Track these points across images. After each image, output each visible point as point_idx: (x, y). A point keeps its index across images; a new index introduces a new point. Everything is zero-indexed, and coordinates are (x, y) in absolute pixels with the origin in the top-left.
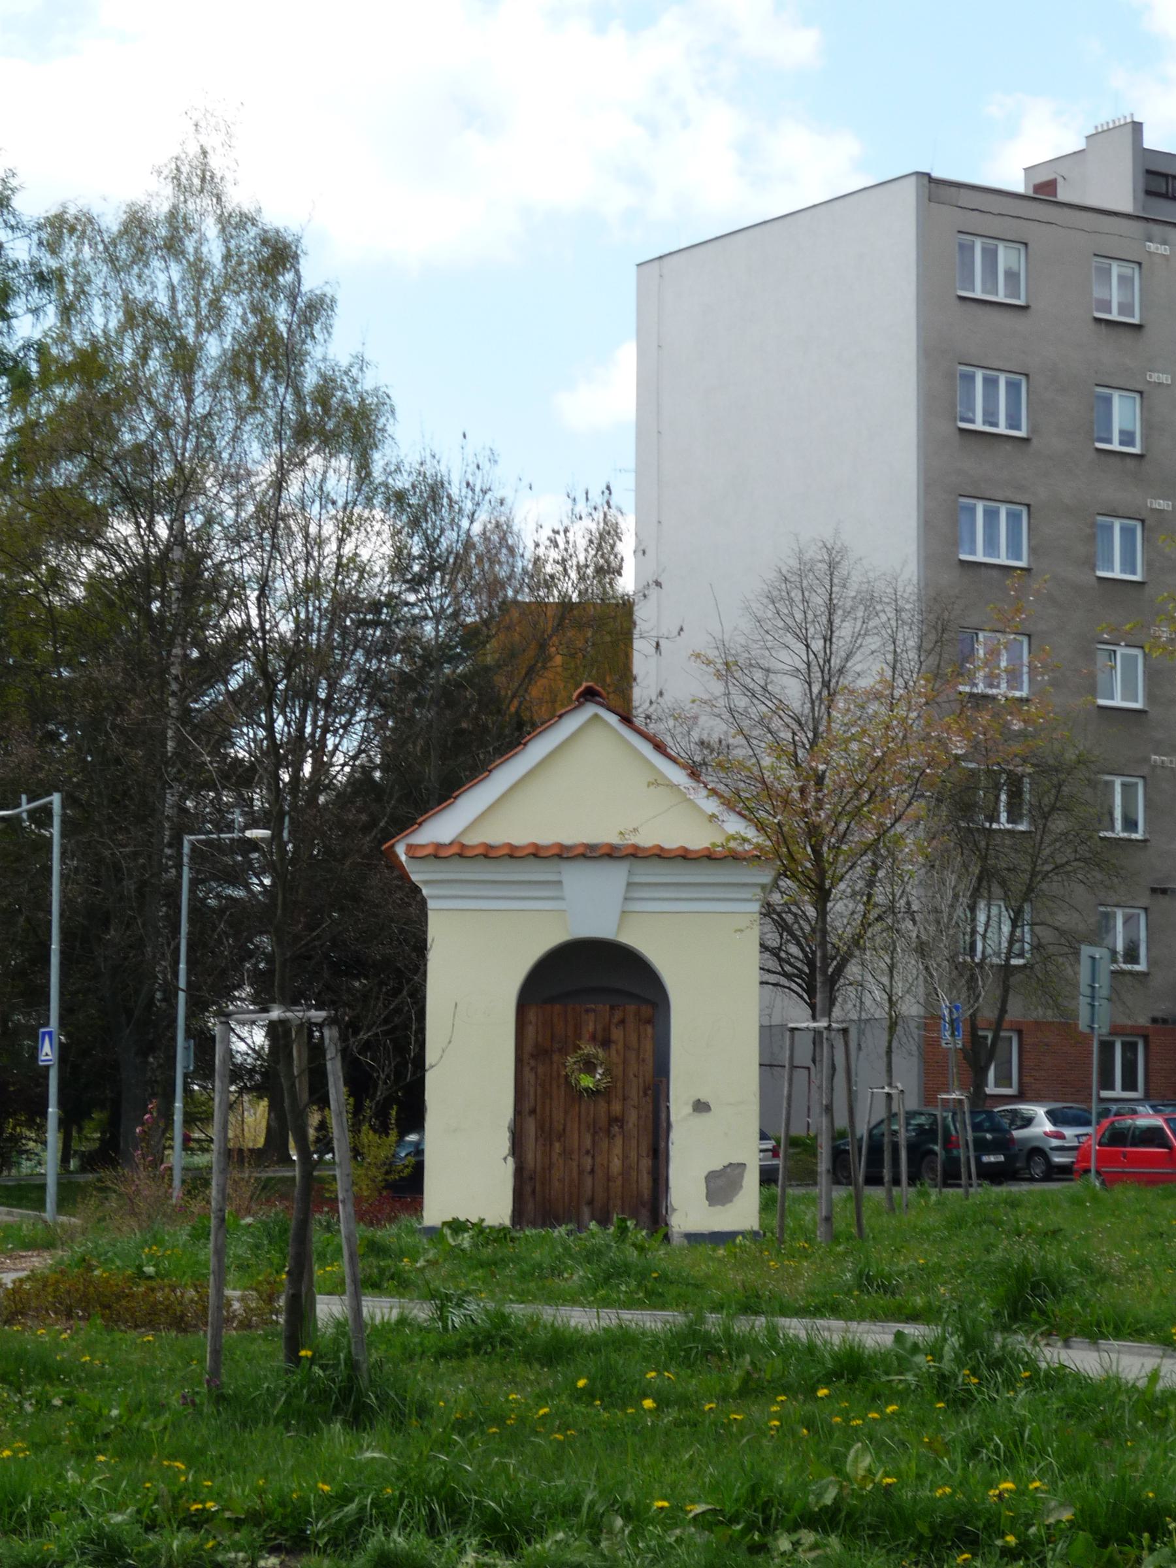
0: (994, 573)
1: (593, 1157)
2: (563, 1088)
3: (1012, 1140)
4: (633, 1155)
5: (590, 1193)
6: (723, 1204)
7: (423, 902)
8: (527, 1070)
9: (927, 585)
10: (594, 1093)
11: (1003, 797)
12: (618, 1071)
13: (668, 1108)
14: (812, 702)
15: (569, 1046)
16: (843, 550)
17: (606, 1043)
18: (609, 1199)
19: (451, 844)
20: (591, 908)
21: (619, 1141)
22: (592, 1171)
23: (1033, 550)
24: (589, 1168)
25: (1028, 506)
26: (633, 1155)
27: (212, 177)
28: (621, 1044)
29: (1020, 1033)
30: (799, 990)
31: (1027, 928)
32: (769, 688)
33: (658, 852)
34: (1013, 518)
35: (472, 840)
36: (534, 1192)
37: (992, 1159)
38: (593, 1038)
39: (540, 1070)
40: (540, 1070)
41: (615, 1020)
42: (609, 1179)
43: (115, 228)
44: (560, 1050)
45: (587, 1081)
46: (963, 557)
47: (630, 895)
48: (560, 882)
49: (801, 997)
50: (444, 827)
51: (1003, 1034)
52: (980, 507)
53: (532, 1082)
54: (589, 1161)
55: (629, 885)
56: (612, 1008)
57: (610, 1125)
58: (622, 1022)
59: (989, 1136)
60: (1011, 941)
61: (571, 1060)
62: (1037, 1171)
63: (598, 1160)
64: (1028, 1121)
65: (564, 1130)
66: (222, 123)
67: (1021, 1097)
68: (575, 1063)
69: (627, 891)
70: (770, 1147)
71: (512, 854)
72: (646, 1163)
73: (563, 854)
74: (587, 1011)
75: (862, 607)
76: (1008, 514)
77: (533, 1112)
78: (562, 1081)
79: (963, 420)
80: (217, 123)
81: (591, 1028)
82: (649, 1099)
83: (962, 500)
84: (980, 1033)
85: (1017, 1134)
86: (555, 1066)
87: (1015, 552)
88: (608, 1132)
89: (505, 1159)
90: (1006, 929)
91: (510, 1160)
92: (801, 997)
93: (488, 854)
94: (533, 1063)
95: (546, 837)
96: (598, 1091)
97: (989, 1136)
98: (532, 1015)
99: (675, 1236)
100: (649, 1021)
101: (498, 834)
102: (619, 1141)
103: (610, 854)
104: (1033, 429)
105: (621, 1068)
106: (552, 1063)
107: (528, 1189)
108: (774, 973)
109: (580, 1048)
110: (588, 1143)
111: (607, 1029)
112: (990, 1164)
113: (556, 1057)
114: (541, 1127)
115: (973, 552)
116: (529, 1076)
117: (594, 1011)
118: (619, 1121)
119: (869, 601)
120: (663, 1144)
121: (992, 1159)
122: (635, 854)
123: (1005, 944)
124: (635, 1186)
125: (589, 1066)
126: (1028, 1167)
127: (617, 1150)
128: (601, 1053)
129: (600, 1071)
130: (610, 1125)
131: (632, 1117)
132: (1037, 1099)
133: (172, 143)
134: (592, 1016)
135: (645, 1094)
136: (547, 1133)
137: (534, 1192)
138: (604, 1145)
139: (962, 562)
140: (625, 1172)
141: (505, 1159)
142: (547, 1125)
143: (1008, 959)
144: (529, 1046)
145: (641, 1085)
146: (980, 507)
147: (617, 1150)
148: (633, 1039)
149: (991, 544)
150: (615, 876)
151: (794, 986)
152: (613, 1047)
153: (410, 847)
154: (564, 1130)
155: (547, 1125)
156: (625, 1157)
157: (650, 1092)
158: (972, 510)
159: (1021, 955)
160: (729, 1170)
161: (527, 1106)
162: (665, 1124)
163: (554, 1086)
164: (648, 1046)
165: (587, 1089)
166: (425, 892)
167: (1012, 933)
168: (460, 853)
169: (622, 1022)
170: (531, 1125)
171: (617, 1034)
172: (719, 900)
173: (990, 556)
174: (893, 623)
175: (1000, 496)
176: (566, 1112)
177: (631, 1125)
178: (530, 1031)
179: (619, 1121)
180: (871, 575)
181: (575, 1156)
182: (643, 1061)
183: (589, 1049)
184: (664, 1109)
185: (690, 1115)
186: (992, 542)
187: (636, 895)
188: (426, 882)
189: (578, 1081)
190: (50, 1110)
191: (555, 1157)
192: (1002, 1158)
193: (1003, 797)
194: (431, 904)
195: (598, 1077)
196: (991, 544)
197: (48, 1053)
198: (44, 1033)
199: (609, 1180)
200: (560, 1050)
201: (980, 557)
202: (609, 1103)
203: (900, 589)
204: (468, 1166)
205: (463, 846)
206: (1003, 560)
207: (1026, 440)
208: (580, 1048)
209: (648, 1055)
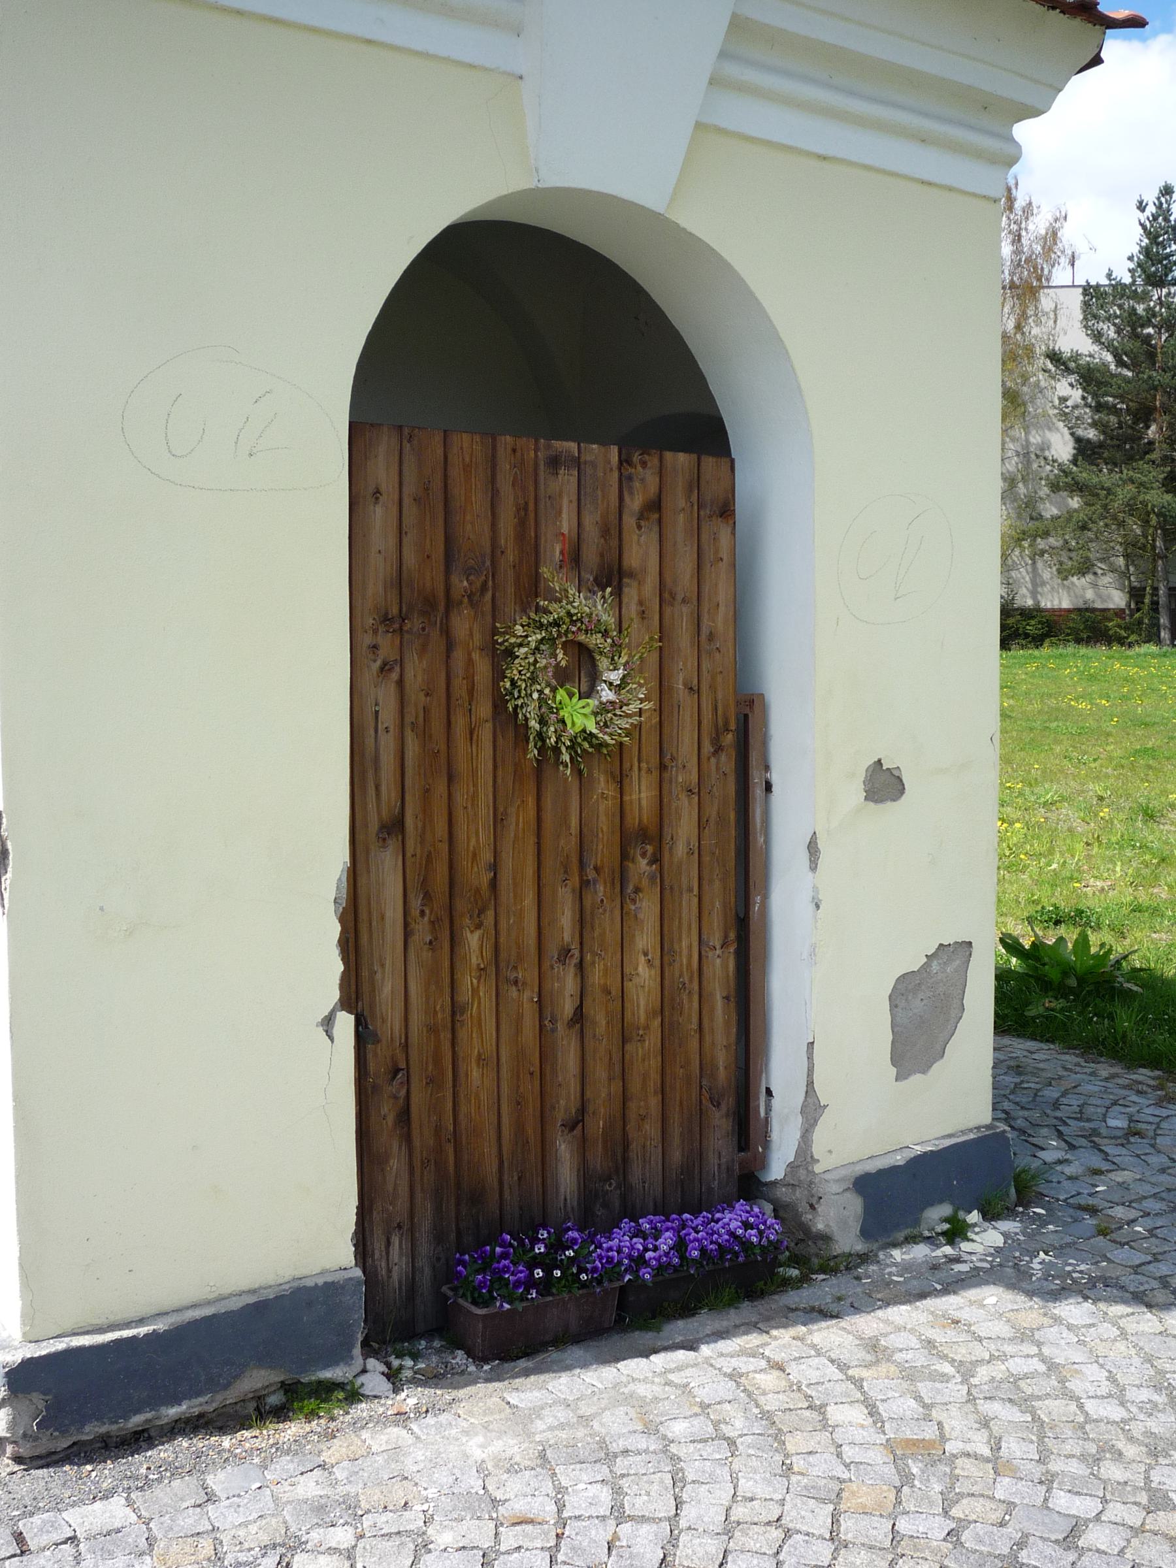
4: (687, 944)
5: (573, 1086)
10: (587, 748)
17: (612, 577)
18: (625, 1099)
21: (647, 908)
22: (579, 1016)
24: (568, 1008)
36: (404, 1116)
54: (570, 984)
58: (655, 506)
63: (596, 976)
65: (494, 884)
72: (721, 965)
74: (555, 463)
81: (566, 524)
89: (328, 1023)
102: (647, 908)
106: (450, 647)
111: (613, 531)
114: (418, 884)
124: (694, 1044)
127: (645, 939)
130: (624, 856)
131: (683, 830)
134: (567, 480)
137: (404, 1116)
138: (607, 924)
140: (667, 1006)
141: (328, 1023)
148: (684, 567)
152: (631, 593)
154: (494, 884)
163: (460, 724)
169: (655, 506)
170: (388, 871)
171: (640, 550)
176: (499, 820)
177: (680, 850)
191: (467, 981)
199: (624, 1040)
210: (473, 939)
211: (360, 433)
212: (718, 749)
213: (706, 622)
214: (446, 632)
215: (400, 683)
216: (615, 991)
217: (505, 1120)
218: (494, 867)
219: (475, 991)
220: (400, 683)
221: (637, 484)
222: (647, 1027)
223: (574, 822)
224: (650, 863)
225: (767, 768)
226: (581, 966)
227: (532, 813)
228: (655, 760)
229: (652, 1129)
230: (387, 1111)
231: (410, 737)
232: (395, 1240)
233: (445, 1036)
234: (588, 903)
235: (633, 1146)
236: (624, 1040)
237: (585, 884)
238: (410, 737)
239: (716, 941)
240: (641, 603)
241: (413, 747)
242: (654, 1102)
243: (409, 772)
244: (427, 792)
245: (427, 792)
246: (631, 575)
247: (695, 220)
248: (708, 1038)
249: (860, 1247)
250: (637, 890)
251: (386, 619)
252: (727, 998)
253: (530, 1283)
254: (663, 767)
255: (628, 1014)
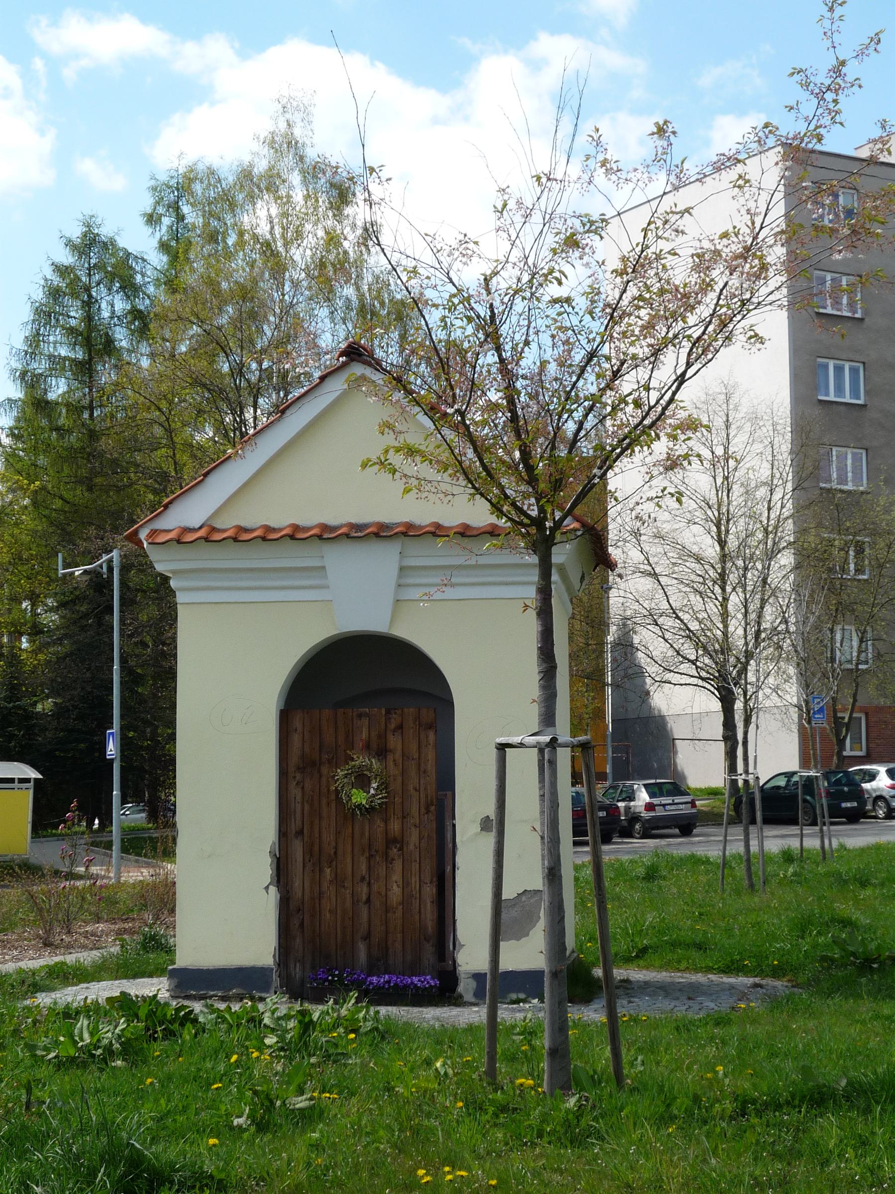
0: (842, 408)
1: (369, 884)
2: (333, 805)
3: (862, 791)
4: (415, 880)
5: (366, 925)
6: (518, 939)
7: (172, 593)
8: (293, 784)
9: (796, 414)
10: (369, 811)
11: (852, 553)
12: (396, 786)
13: (454, 826)
14: (717, 491)
15: (339, 758)
16: (735, 386)
17: (382, 753)
18: (387, 932)
19: (201, 528)
20: (359, 598)
21: (398, 865)
22: (368, 901)
23: (867, 392)
24: (364, 898)
25: (864, 363)
26: (415, 880)
27: (296, 143)
28: (399, 753)
29: (867, 714)
30: (712, 689)
31: (869, 643)
32: (686, 480)
33: (432, 529)
34: (854, 372)
35: (228, 522)
36: (302, 925)
37: (849, 805)
38: (367, 747)
39: (306, 785)
40: (308, 785)
41: (393, 726)
42: (387, 909)
43: (231, 179)
44: (329, 761)
45: (359, 797)
46: (821, 398)
47: (402, 581)
48: (324, 568)
49: (713, 693)
50: (191, 511)
51: (855, 715)
52: (831, 364)
53: (299, 798)
54: (365, 889)
55: (402, 569)
56: (388, 712)
57: (387, 847)
58: (400, 727)
59: (846, 789)
60: (860, 652)
61: (341, 773)
62: (881, 813)
63: (375, 887)
64: (872, 776)
65: (335, 853)
66: (301, 105)
67: (868, 758)
68: (346, 776)
69: (400, 576)
70: (690, 800)
71: (267, 536)
72: (430, 891)
73: (326, 534)
74: (360, 716)
75: (749, 424)
76: (850, 369)
77: (300, 833)
78: (333, 797)
79: (818, 307)
80: (298, 106)
81: (364, 735)
82: (432, 817)
83: (819, 360)
84: (839, 715)
85: (866, 786)
86: (324, 779)
87: (855, 393)
88: (386, 855)
89: (267, 888)
90: (855, 643)
91: (273, 890)
92: (713, 693)
93: (239, 537)
94: (299, 776)
95: (310, 518)
96: (372, 808)
97: (846, 789)
98: (297, 722)
99: (463, 976)
100: (430, 726)
101: (255, 514)
102: (398, 865)
103: (380, 533)
104: (866, 312)
105: (399, 779)
106: (321, 776)
107: (295, 922)
108: (692, 676)
109: (353, 759)
110: (364, 868)
111: (382, 736)
112: (847, 808)
113: (325, 770)
114: (309, 851)
115: (827, 394)
116: (295, 792)
117: (367, 715)
118: (399, 842)
119: (754, 419)
120: (449, 869)
121: (849, 805)
122: (408, 532)
123: (855, 654)
124: (417, 917)
125: (362, 781)
126: (874, 810)
127: (397, 877)
128: (375, 764)
129: (375, 785)
130: (387, 847)
131: (413, 838)
132: (880, 761)
133: (267, 123)
134: (365, 721)
135: (428, 811)
136: (316, 858)
137: (302, 925)
138: (382, 871)
139: (820, 401)
140: (406, 901)
141: (267, 888)
142: (316, 848)
143: (857, 664)
144: (294, 759)
145: (423, 801)
146: (831, 364)
147: (397, 877)
148: (414, 746)
149: (839, 389)
150: (384, 559)
151: (709, 687)
152: (390, 757)
153: (154, 533)
154: (335, 853)
155: (316, 848)
156: (405, 884)
157: (433, 808)
158: (826, 367)
159: (867, 662)
160: (524, 898)
161: (294, 827)
162: (451, 845)
163: (324, 802)
164: (430, 754)
165: (359, 806)
166: (173, 583)
167: (860, 646)
168: (210, 535)
169: (400, 727)
170: (298, 849)
171: (394, 742)
172: (507, 584)
173: (839, 397)
174: (771, 433)
175: (844, 357)
176: (338, 833)
177: (411, 847)
178: (296, 740)
179: (396, 842)
180: (755, 402)
181: (348, 884)
182: (425, 772)
183: (361, 760)
184: (450, 828)
185: (477, 834)
186: (841, 388)
187: (411, 581)
188: (174, 572)
189: (349, 798)
190: (114, 793)
191: (325, 885)
192: (855, 804)
193: (852, 553)
194: (180, 598)
195: (372, 791)
196: (839, 389)
197: (112, 749)
198: (110, 734)
199: (387, 911)
200: (329, 761)
201: (832, 397)
202: (386, 821)
203: (775, 409)
204: (224, 895)
205: (214, 530)
206: (847, 399)
207: (861, 320)
208: (353, 759)
209: (431, 767)
210: (328, 871)
211: (285, 717)
212: (428, 812)
213: (423, 765)
214: (319, 771)
215: (303, 788)
216: (383, 893)
217: (339, 932)
218: (336, 848)
219: (328, 888)
220: (303, 788)
221: (392, 720)
222: (397, 908)
223: (367, 834)
224: (399, 850)
225: (454, 818)
226: (369, 884)
227: (350, 831)
228: (400, 815)
229: (398, 946)
230: (295, 922)
231: (306, 804)
232: (298, 965)
233: (317, 901)
234: (372, 863)
235: (390, 950)
236: (387, 911)
237: (371, 856)
238: (306, 804)
239: (428, 880)
240: (394, 761)
241: (307, 807)
242: (399, 936)
243: (306, 815)
244: (312, 823)
245: (312, 823)
246: (391, 751)
247: (403, 631)
248: (423, 916)
249: (473, 1000)
250: (393, 859)
251: (298, 768)
252: (433, 902)
253: (326, 980)
254: (404, 817)
255: (389, 901)
